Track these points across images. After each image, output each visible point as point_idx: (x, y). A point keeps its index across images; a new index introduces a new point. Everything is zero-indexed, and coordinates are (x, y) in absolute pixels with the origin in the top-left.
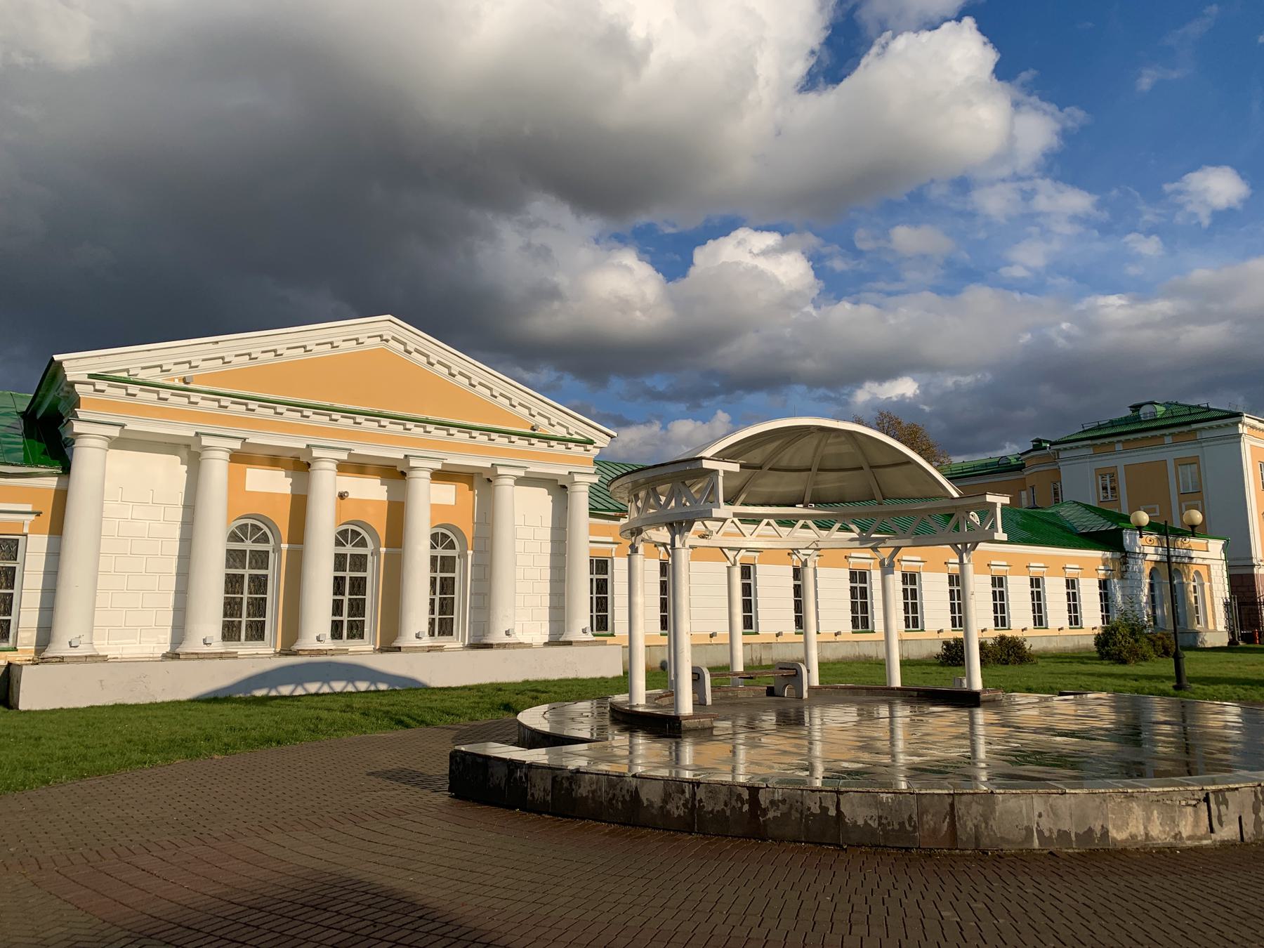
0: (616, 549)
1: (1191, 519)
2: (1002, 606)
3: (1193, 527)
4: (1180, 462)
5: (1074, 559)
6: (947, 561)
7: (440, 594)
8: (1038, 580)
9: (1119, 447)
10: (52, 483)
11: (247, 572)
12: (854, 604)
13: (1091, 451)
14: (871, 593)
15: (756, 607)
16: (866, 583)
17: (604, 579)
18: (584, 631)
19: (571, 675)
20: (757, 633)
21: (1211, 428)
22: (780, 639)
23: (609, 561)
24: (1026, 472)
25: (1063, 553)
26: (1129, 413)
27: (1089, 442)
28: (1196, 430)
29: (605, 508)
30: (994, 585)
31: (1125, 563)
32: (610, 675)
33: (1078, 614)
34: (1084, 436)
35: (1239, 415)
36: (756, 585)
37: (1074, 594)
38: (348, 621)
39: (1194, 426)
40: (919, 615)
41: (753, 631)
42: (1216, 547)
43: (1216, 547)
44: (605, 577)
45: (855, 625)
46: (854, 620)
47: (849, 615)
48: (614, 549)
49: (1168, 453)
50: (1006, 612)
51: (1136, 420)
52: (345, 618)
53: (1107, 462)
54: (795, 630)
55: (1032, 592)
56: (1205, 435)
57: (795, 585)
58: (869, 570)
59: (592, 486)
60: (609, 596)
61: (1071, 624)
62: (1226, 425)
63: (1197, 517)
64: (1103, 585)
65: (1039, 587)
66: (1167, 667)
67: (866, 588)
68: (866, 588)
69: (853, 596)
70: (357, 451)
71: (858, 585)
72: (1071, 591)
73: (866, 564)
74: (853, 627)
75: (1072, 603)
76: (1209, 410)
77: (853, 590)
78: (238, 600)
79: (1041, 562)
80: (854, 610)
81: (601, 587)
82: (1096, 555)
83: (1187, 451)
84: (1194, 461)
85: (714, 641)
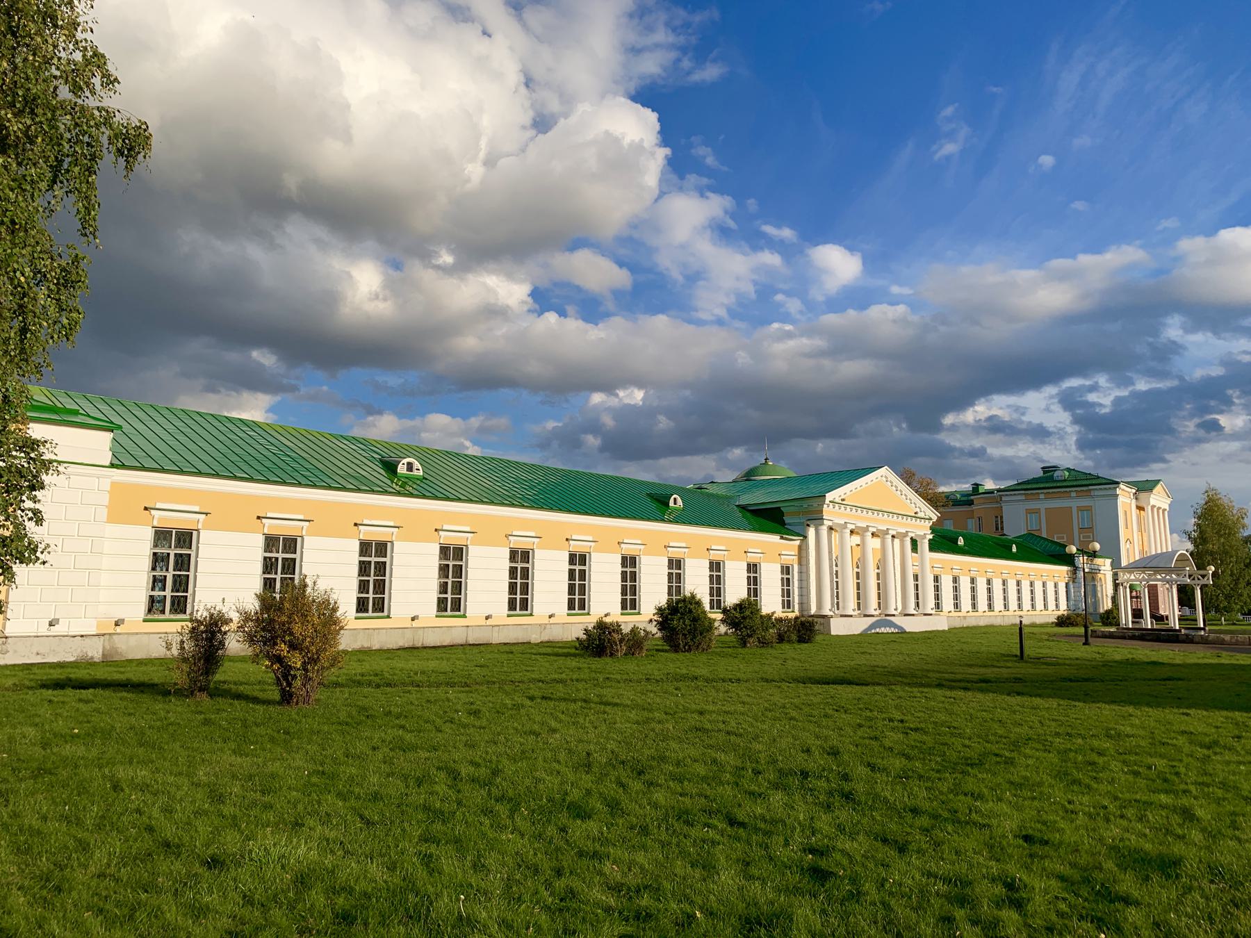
0: (308, 527)
1: (1094, 547)
2: (755, 590)
3: (1095, 552)
4: (1080, 509)
5: (680, 537)
6: (569, 537)
7: (174, 570)
8: (718, 564)
9: (1042, 496)
10: (798, 543)
11: (451, 563)
12: (670, 588)
13: (1023, 497)
14: (724, 580)
15: (590, 591)
16: (680, 569)
17: (382, 562)
18: (875, 610)
19: (935, 629)
20: (388, 617)
21: (1101, 489)
22: (552, 620)
23: (299, 540)
24: (974, 507)
25: (218, 488)
26: (1041, 474)
27: (1023, 492)
28: (1090, 490)
29: (430, 495)
30: (711, 569)
31: (1076, 573)
32: (940, 629)
33: (791, 599)
34: (1020, 487)
35: (1118, 483)
36: (724, 576)
37: (755, 578)
38: (172, 596)
39: (1091, 487)
40: (637, 597)
41: (637, 611)
42: (1108, 561)
43: (1108, 561)
44: (460, 563)
45: (624, 607)
46: (624, 603)
47: (619, 597)
48: (305, 527)
49: (1073, 503)
50: (530, 593)
51: (1051, 479)
52: (449, 596)
53: (1033, 505)
54: (781, 610)
55: (782, 579)
56: (1097, 493)
57: (570, 570)
58: (589, 553)
59: (930, 540)
60: (191, 574)
61: (783, 607)
62: (1110, 488)
63: (1097, 546)
64: (1067, 585)
65: (789, 574)
66: (1081, 630)
67: (585, 570)
68: (585, 570)
69: (670, 580)
70: (836, 522)
71: (675, 571)
72: (752, 575)
73: (636, 549)
74: (622, 609)
75: (785, 588)
76: (1098, 477)
77: (670, 575)
78: (184, 579)
79: (683, 542)
80: (624, 592)
81: (937, 588)
82: (1065, 568)
83: (1084, 502)
84: (1089, 509)
85: (415, 624)
